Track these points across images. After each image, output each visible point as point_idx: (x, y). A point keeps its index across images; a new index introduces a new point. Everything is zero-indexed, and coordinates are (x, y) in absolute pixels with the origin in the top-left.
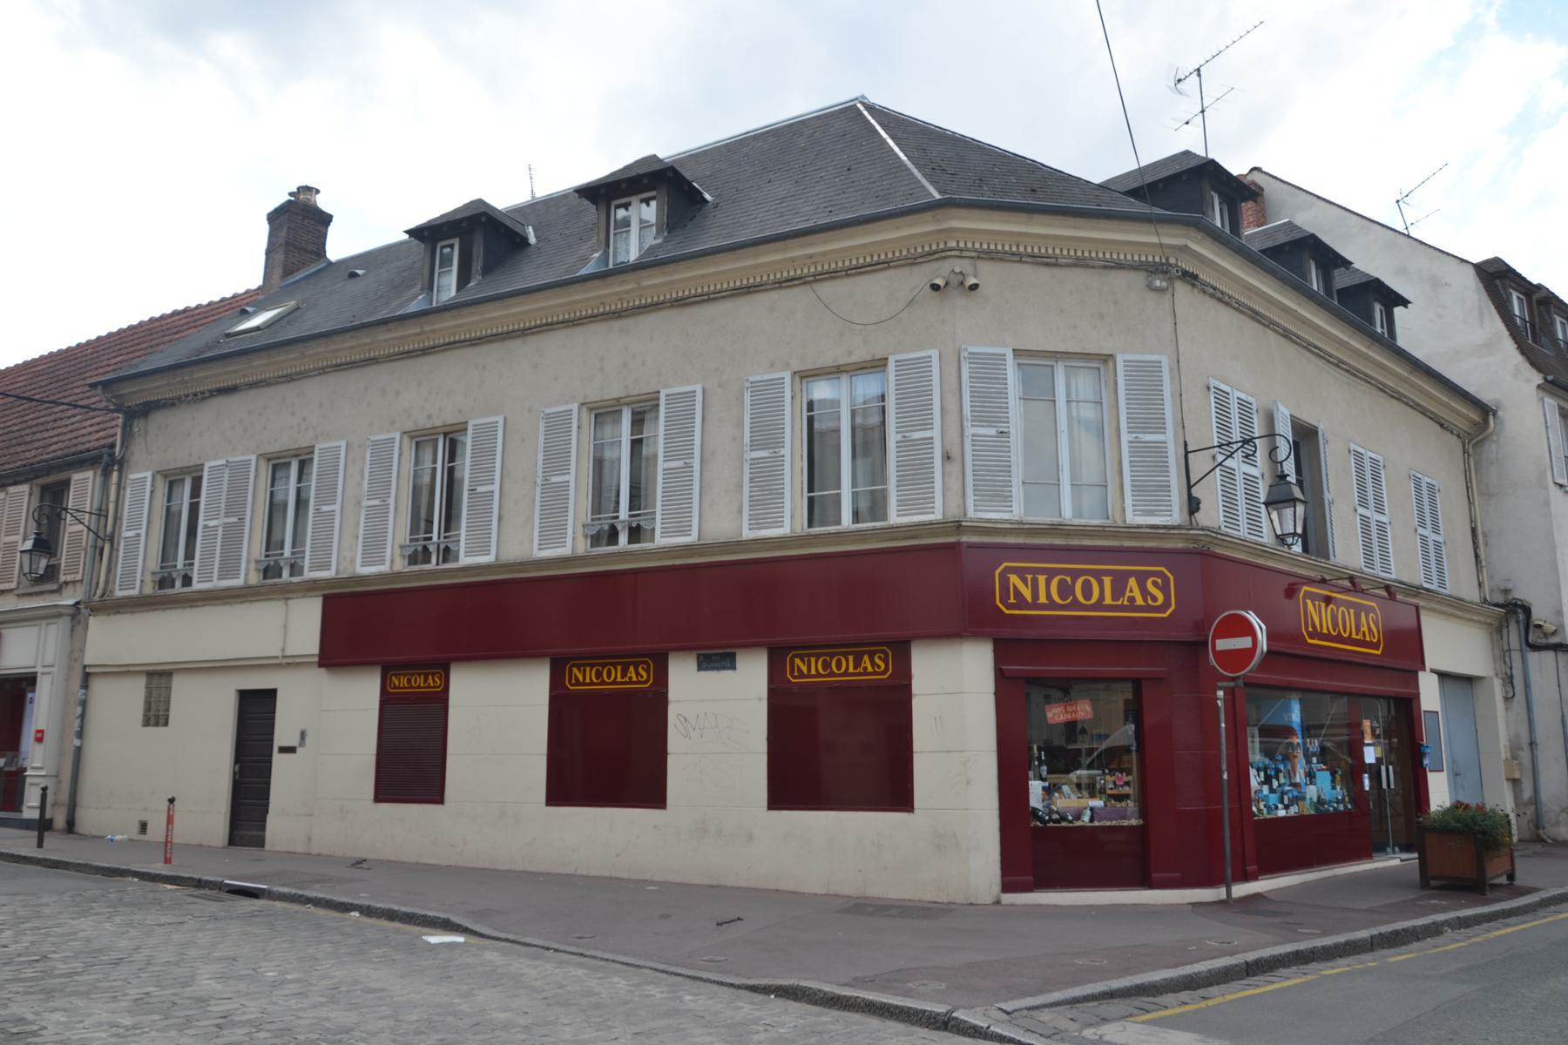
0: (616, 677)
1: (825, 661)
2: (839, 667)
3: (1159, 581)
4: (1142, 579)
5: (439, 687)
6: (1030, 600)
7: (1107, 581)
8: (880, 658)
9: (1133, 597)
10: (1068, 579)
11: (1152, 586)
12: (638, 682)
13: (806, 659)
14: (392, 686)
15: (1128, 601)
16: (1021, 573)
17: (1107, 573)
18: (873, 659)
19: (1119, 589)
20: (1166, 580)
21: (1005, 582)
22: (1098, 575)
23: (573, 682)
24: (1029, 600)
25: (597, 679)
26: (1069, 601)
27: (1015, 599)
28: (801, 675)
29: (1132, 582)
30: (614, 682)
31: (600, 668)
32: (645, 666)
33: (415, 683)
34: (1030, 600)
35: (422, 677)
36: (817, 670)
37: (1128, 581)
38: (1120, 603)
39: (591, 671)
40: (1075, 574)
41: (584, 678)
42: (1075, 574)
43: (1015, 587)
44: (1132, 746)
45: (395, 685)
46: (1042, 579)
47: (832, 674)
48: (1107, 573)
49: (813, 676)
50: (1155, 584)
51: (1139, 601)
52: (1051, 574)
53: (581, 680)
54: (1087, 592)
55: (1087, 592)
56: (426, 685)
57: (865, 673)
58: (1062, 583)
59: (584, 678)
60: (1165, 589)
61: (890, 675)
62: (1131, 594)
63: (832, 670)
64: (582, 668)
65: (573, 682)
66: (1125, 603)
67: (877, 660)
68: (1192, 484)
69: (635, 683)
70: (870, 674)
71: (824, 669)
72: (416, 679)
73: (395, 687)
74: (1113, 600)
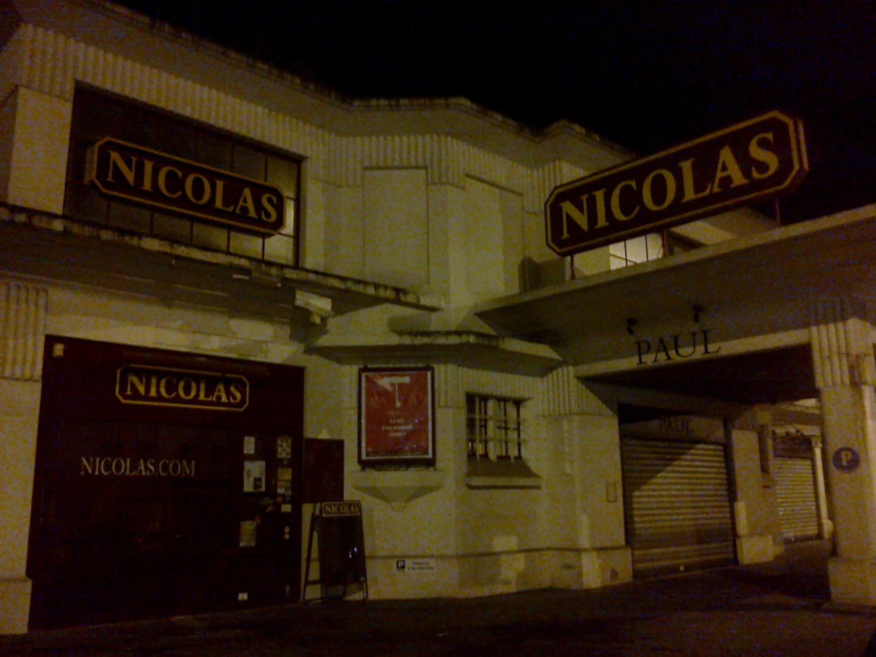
0: (197, 395)
7: (220, 185)
8: (764, 144)
10: (633, 184)
11: (266, 201)
14: (326, 512)
15: (240, 210)
16: (126, 155)
18: (747, 153)
24: (585, 227)
25: (625, 212)
26: (175, 196)
27: (113, 178)
29: (726, 155)
31: (633, 184)
32: (770, 136)
33: (343, 510)
35: (686, 166)
36: (158, 391)
37: (242, 191)
38: (707, 192)
39: (100, 462)
40: (188, 169)
41: (94, 470)
42: (188, 169)
43: (114, 162)
45: (328, 512)
46: (148, 166)
47: (178, 399)
51: (252, 213)
53: (585, 227)
54: (659, 191)
57: (219, 402)
58: (170, 176)
59: (94, 470)
60: (780, 147)
61: (247, 408)
62: (724, 174)
63: (178, 394)
64: (584, 198)
66: (716, 189)
68: (624, 257)
70: (224, 404)
74: (223, 205)
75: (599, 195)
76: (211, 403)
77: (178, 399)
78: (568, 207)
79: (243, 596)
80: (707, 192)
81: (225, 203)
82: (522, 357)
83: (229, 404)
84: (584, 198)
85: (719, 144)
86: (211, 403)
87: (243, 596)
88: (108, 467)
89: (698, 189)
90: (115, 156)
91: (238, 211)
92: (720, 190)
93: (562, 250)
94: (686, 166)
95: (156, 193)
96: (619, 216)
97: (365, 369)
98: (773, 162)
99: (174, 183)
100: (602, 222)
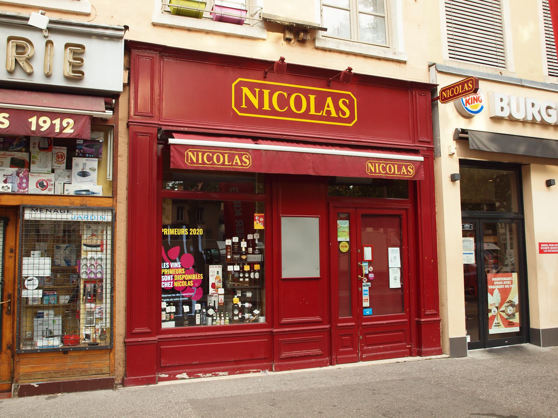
2: (299, 106)
3: (347, 101)
4: (336, 98)
6: (257, 108)
7: (312, 98)
9: (330, 111)
12: (339, 119)
16: (251, 87)
17: (313, 92)
20: (352, 101)
22: (306, 93)
25: (452, 95)
28: (250, 108)
31: (285, 94)
34: (257, 108)
38: (320, 114)
40: (291, 91)
46: (266, 92)
49: (266, 113)
50: (344, 103)
52: (273, 89)
57: (328, 117)
58: (280, 97)
63: (290, 108)
66: (324, 114)
69: (334, 120)
70: (406, 175)
72: (457, 89)
75: (448, 91)
76: (321, 118)
77: (290, 113)
78: (443, 93)
82: (427, 351)
83: (339, 119)
84: (446, 91)
85: (403, 165)
86: (321, 118)
88: (384, 169)
89: (462, 91)
90: (246, 91)
91: (324, 114)
93: (442, 102)
95: (273, 112)
96: (457, 87)
97: (205, 324)
99: (283, 102)
100: (448, 96)
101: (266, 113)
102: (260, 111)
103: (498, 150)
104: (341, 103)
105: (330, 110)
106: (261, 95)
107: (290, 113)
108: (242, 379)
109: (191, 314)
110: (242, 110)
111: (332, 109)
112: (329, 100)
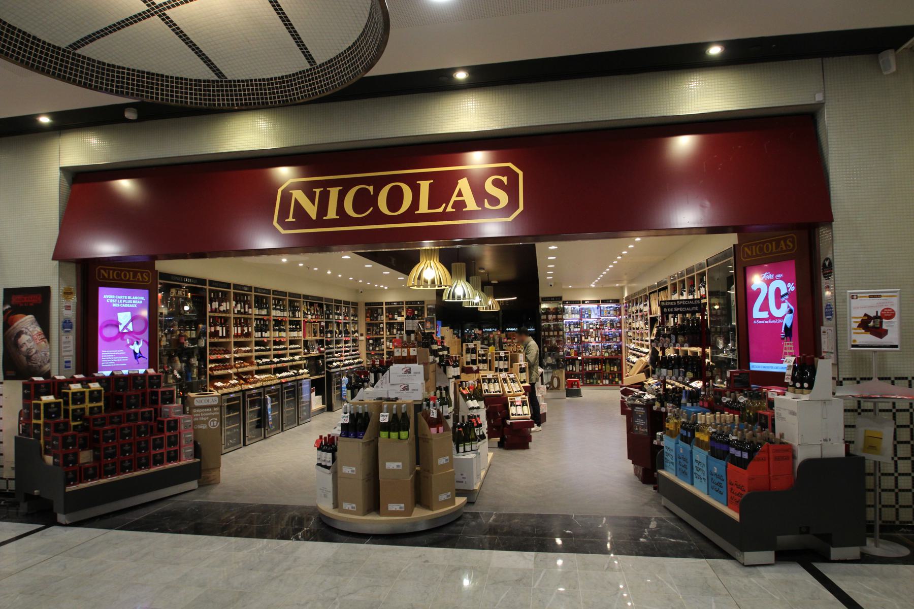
1: (117, 273)
4: (142, 273)
5: (792, 250)
7: (131, 273)
9: (463, 201)
10: (371, 188)
13: (318, 191)
16: (105, 270)
17: (132, 271)
19: (135, 276)
20: (149, 274)
21: (743, 250)
22: (129, 271)
23: (746, 256)
28: (749, 256)
29: (782, 242)
30: (771, 253)
32: (505, 179)
35: (774, 243)
36: (756, 252)
38: (440, 210)
39: (772, 250)
40: (122, 271)
41: (752, 253)
42: (122, 271)
44: (121, 324)
46: (111, 272)
48: (132, 271)
49: (111, 280)
50: (790, 241)
52: (114, 270)
55: (395, 199)
56: (779, 249)
57: (138, 281)
58: (117, 273)
59: (752, 253)
60: (793, 242)
65: (746, 256)
66: (449, 209)
67: (145, 276)
69: (785, 251)
70: (785, 251)
71: (358, 206)
73: (749, 256)
79: (301, 265)
80: (440, 210)
81: (133, 278)
87: (301, 265)
89: (776, 249)
90: (102, 271)
92: (509, 424)
94: (774, 243)
95: (114, 279)
98: (791, 245)
101: (111, 280)
102: (321, 221)
103: (17, 325)
104: (144, 275)
105: (464, 201)
106: (752, 248)
107: (121, 280)
108: (240, 440)
109: (251, 399)
110: (745, 258)
111: (140, 277)
112: (139, 274)
